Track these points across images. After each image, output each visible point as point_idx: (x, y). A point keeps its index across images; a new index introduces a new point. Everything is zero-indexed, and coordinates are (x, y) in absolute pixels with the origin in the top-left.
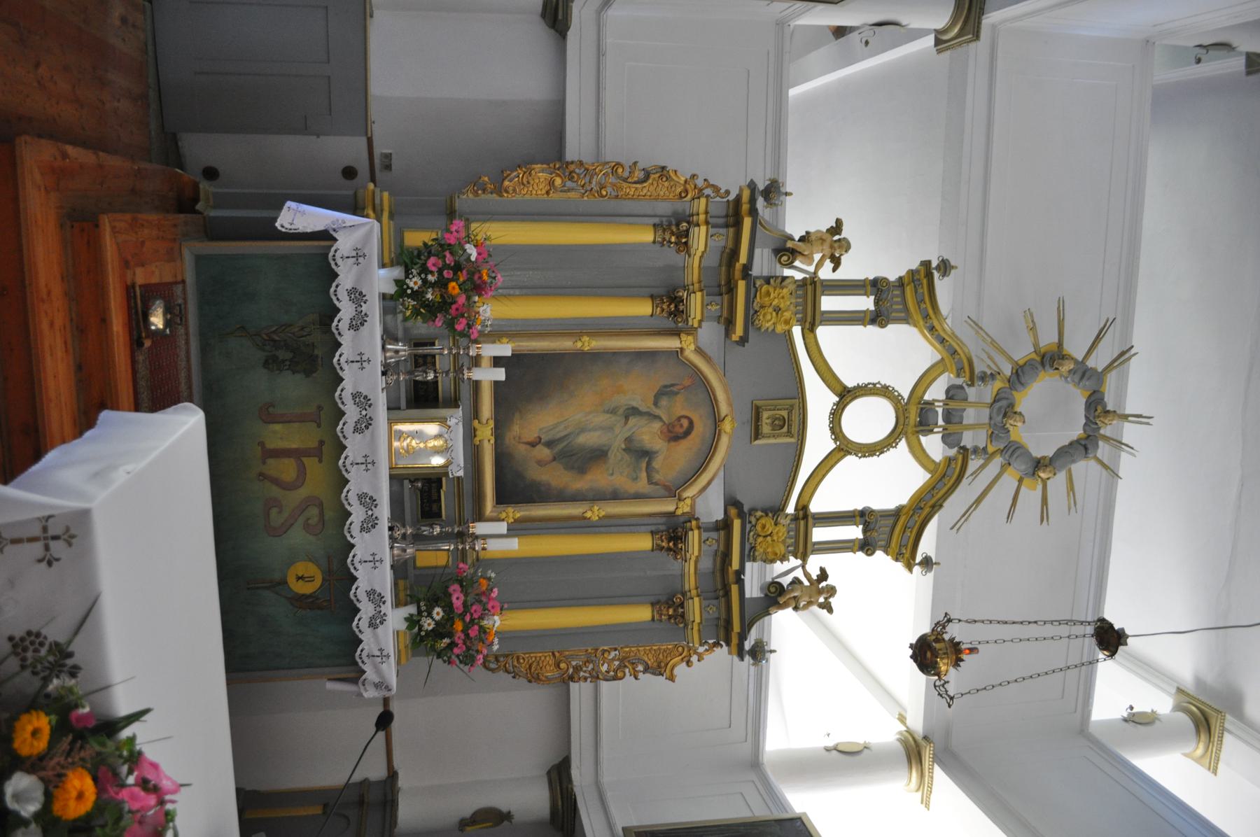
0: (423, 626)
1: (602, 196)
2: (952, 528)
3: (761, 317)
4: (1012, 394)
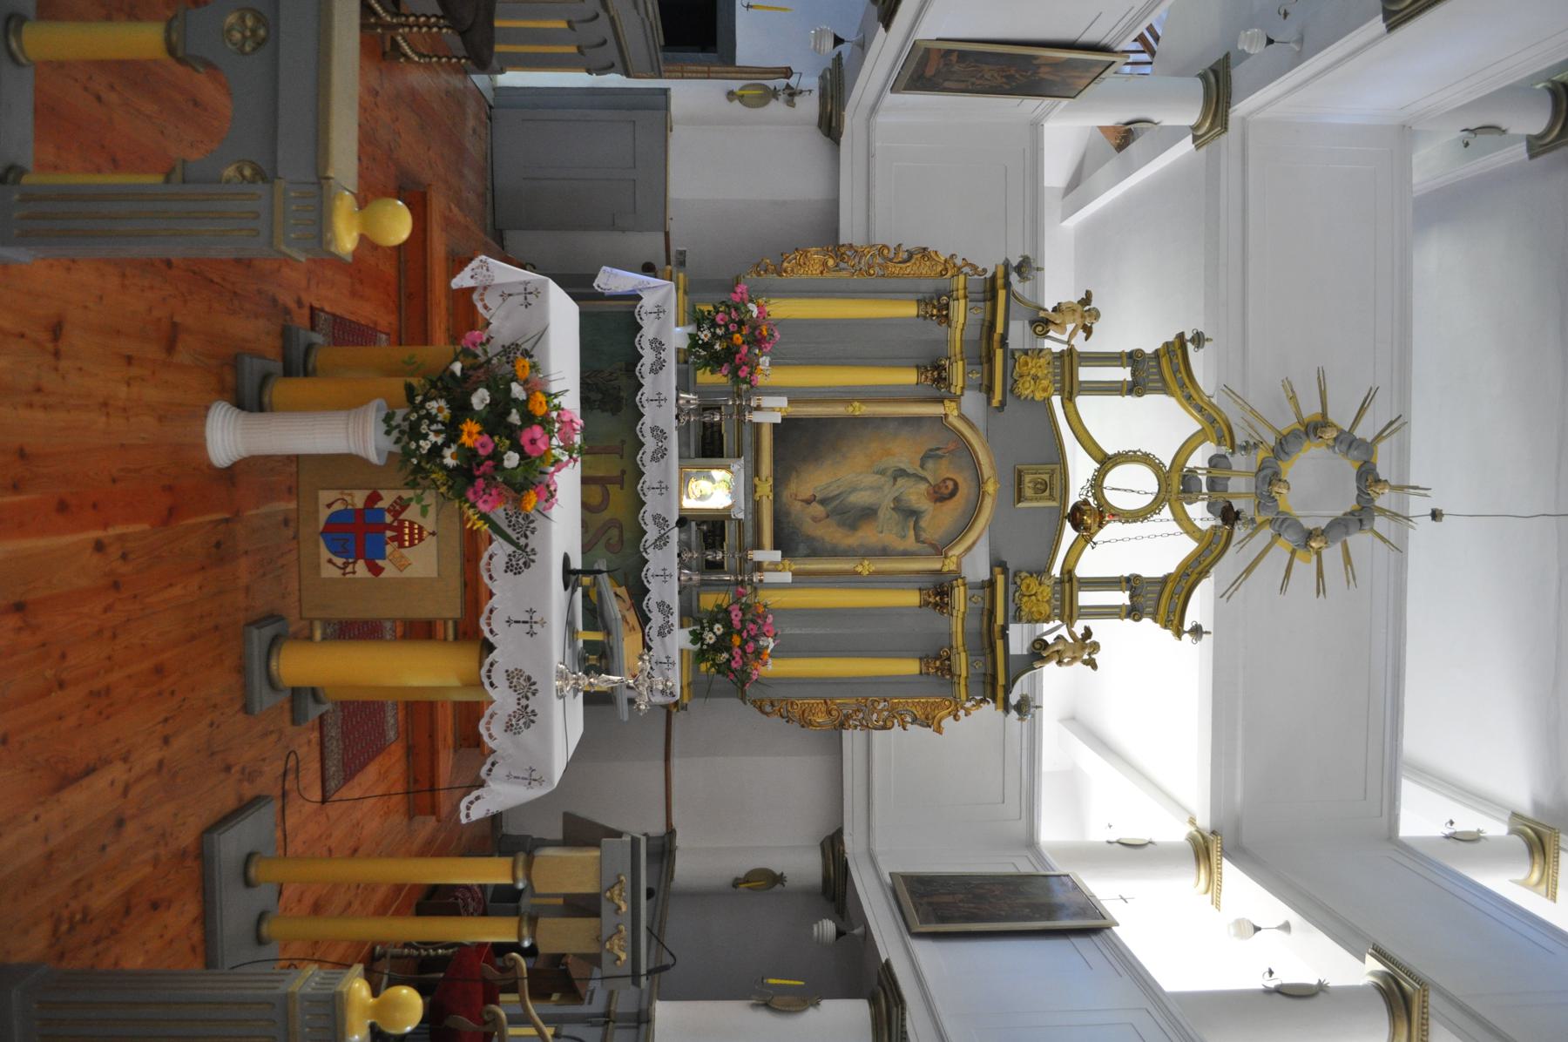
0: (705, 639)
1: (870, 275)
2: (1222, 597)
3: (1020, 386)
4: (1277, 463)
